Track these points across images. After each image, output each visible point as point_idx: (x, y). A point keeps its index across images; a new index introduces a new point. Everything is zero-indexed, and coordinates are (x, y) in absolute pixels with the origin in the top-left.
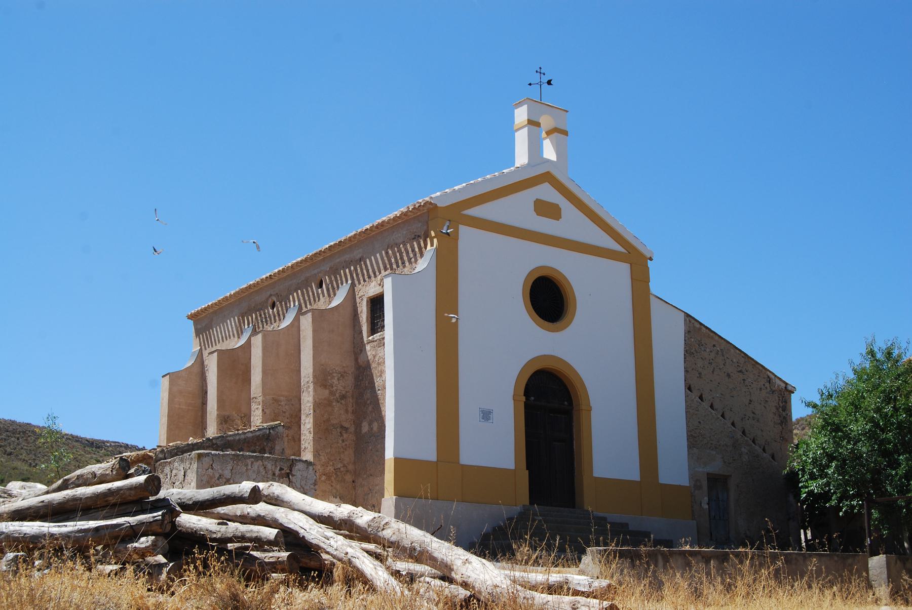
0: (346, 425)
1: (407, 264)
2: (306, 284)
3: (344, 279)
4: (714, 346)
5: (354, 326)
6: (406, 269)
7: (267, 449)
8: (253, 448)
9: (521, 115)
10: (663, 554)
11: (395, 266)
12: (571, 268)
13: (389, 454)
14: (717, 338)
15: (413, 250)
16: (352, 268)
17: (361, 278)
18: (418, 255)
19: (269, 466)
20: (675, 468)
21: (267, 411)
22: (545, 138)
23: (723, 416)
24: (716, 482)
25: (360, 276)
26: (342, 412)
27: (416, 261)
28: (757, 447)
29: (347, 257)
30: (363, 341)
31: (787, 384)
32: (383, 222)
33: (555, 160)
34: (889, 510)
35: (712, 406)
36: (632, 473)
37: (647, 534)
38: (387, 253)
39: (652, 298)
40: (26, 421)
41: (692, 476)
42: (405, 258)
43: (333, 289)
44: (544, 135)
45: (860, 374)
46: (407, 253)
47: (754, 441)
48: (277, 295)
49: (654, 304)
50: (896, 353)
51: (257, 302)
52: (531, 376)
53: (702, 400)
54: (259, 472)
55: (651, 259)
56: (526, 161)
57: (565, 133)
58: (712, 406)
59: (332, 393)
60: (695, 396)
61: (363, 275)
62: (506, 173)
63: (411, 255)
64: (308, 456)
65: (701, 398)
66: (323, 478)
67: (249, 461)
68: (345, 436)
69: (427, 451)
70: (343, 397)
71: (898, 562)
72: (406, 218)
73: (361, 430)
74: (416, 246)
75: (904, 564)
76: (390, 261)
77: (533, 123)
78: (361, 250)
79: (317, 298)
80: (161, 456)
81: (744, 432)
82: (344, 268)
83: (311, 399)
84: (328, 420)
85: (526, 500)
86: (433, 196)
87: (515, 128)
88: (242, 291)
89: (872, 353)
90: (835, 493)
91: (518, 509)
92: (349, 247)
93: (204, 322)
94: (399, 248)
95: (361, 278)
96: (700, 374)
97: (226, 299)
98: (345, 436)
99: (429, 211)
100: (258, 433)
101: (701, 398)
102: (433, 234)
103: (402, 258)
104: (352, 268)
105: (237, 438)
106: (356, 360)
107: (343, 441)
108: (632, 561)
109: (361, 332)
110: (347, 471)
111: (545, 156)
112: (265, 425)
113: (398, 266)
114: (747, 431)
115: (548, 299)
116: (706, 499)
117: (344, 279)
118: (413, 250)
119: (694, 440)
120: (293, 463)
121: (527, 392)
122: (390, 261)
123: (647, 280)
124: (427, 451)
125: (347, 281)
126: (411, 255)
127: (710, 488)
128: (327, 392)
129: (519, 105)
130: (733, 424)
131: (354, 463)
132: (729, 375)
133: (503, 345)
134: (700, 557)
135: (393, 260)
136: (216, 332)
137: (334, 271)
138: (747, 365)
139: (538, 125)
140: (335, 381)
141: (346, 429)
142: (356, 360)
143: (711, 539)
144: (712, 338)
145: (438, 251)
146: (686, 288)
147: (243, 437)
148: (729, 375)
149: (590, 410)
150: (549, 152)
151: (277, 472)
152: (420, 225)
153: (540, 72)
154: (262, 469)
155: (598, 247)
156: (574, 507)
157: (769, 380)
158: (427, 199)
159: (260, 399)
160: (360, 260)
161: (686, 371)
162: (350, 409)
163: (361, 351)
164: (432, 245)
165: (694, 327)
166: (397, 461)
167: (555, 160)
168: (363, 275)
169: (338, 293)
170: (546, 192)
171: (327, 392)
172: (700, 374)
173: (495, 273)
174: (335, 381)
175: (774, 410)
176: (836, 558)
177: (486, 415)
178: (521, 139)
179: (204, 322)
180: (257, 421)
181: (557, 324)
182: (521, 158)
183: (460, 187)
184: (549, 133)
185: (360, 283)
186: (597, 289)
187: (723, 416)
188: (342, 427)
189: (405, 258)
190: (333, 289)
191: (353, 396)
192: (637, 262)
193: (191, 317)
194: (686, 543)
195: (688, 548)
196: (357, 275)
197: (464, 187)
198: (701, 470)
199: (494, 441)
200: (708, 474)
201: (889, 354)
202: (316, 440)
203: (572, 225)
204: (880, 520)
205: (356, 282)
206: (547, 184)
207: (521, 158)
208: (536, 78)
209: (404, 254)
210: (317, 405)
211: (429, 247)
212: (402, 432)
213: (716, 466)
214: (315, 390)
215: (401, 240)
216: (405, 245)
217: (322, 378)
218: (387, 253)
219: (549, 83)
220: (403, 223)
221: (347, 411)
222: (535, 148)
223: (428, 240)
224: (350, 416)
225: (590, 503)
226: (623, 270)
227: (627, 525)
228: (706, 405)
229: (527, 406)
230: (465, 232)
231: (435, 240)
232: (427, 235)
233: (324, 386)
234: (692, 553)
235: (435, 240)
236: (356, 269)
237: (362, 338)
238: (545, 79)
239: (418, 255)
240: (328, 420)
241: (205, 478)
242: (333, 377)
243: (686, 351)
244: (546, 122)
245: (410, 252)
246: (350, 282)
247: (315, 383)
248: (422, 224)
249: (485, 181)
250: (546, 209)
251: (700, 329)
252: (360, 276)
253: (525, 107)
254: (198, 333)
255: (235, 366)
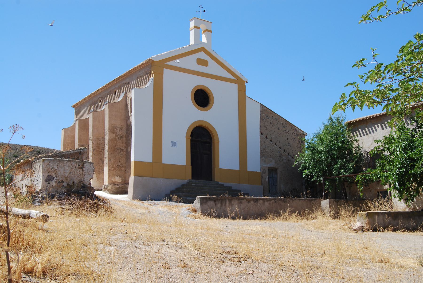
0: (123, 148)
2: (110, 93)
7: (80, 157)
8: (74, 157)
9: (192, 24)
10: (229, 199)
13: (132, 160)
15: (146, 79)
19: (74, 164)
20: (255, 164)
21: (95, 143)
23: (276, 144)
24: (272, 171)
27: (147, 83)
28: (290, 157)
29: (124, 82)
31: (303, 132)
34: (332, 181)
35: (271, 141)
36: (236, 167)
37: (239, 191)
38: (137, 80)
39: (247, 98)
41: (261, 168)
42: (143, 82)
44: (202, 32)
45: (326, 128)
47: (288, 154)
48: (101, 98)
49: (247, 100)
50: (341, 119)
51: (94, 100)
52: (193, 130)
54: (69, 166)
55: (247, 82)
56: (193, 43)
57: (211, 31)
58: (271, 141)
59: (117, 136)
60: (264, 137)
62: (185, 48)
64: (90, 160)
65: (266, 137)
66: (113, 169)
67: (65, 162)
68: (122, 152)
69: (148, 158)
70: (121, 137)
71: (335, 202)
75: (337, 203)
77: (196, 27)
79: (114, 99)
80: (34, 160)
81: (284, 151)
82: (123, 86)
83: (108, 138)
84: (115, 146)
88: (92, 94)
89: (331, 119)
90: (315, 175)
91: (187, 181)
93: (78, 108)
97: (84, 99)
98: (122, 152)
100: (76, 151)
101: (266, 137)
103: (142, 82)
105: (67, 153)
106: (127, 124)
107: (121, 154)
108: (5, 187)
109: (128, 112)
112: (79, 148)
114: (286, 151)
115: (202, 98)
116: (268, 177)
118: (146, 79)
119: (263, 154)
120: (84, 163)
121: (192, 135)
123: (245, 91)
124: (148, 158)
127: (270, 173)
128: (115, 135)
129: (191, 20)
133: (181, 117)
134: (245, 200)
136: (82, 112)
137: (120, 88)
138: (286, 124)
139: (199, 28)
140: (118, 131)
141: (122, 150)
142: (127, 122)
143: (269, 193)
145: (154, 79)
146: (265, 93)
147: (69, 153)
148: (278, 128)
150: (204, 40)
151: (77, 167)
153: (385, 2)
154: (70, 165)
157: (296, 131)
158: (150, 58)
159: (92, 138)
161: (260, 127)
162: (124, 142)
166: (135, 162)
169: (121, 96)
170: (202, 55)
171: (115, 135)
173: (178, 88)
175: (298, 142)
176: (307, 201)
177: (174, 144)
178: (192, 34)
179: (78, 108)
180: (77, 147)
182: (192, 41)
184: (204, 32)
187: (276, 144)
188: (121, 149)
189: (143, 82)
192: (241, 84)
193: (74, 106)
194: (241, 194)
195: (242, 197)
199: (177, 154)
201: (338, 120)
202: (110, 154)
203: (213, 68)
204: (329, 186)
207: (192, 41)
210: (110, 141)
211: (151, 77)
212: (140, 150)
213: (272, 164)
214: (109, 134)
215: (142, 75)
216: (143, 77)
217: (112, 130)
218: (137, 80)
219: (204, 11)
221: (123, 143)
222: (198, 37)
224: (124, 145)
225: (217, 177)
227: (231, 187)
228: (269, 140)
229: (192, 140)
230: (166, 71)
231: (153, 75)
232: (151, 73)
233: (114, 133)
235: (153, 75)
236: (127, 87)
238: (203, 10)
240: (115, 146)
241: (46, 169)
243: (261, 119)
244: (203, 27)
247: (109, 132)
249: (175, 51)
250: (201, 62)
253: (193, 21)
254: (76, 112)
255: (84, 125)
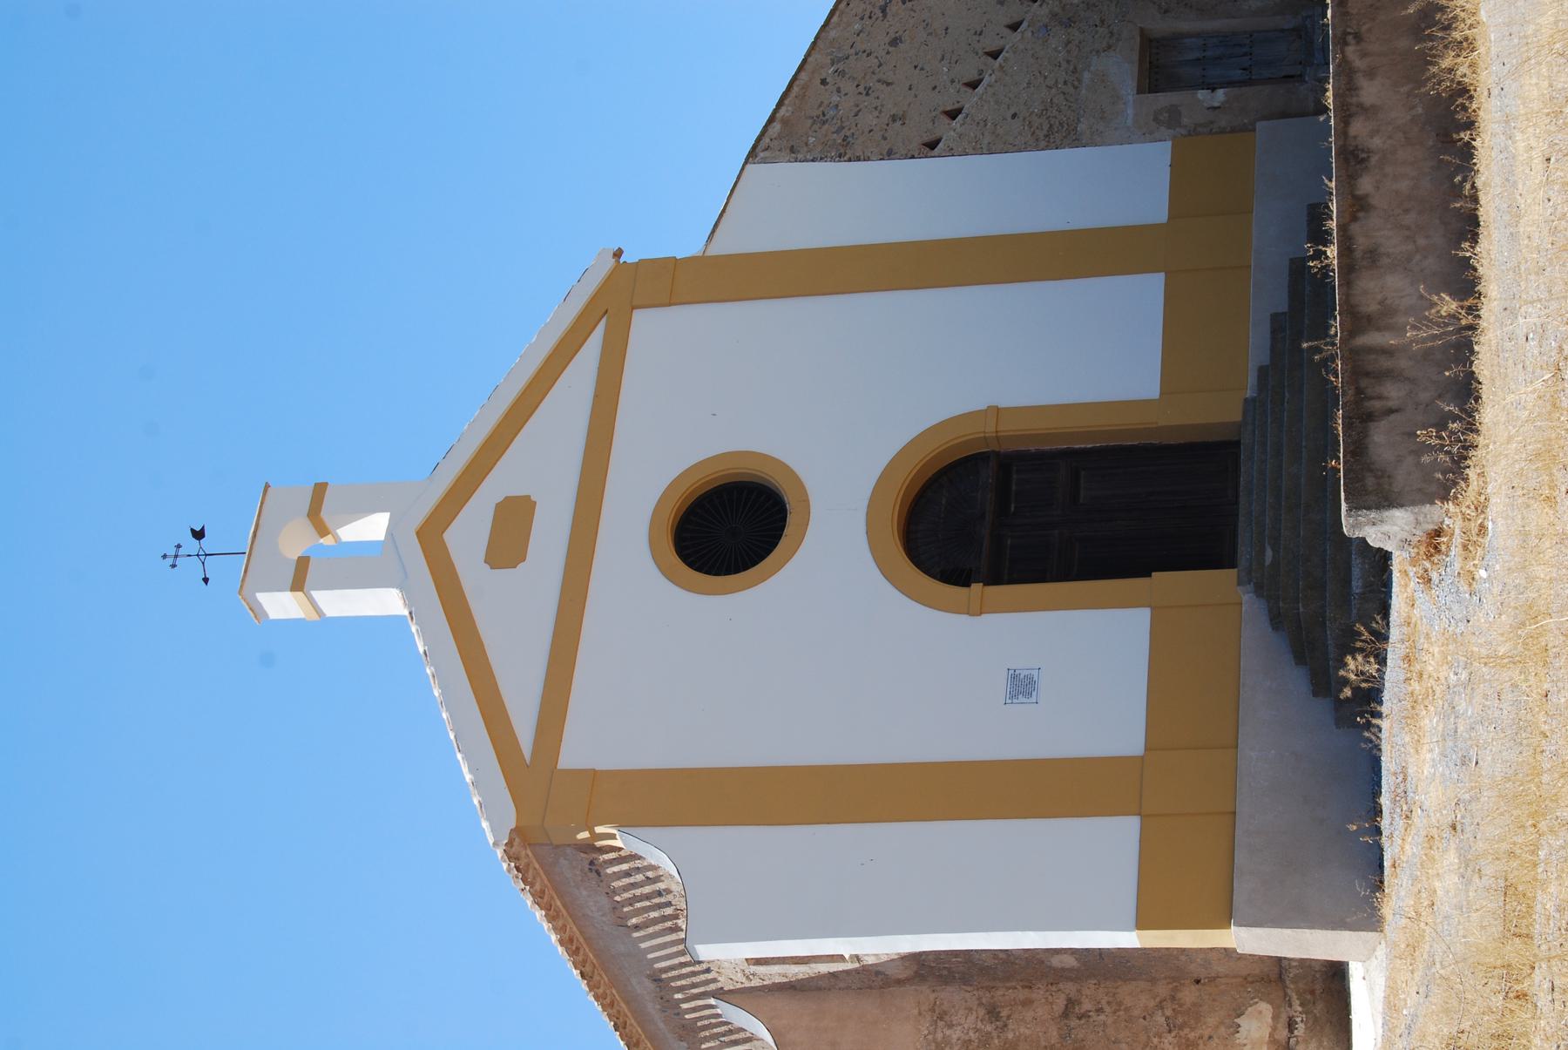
0: (1061, 1003)
1: (661, 886)
3: (707, 1012)
4: (824, 82)
5: (819, 989)
6: (674, 887)
9: (281, 605)
11: (669, 911)
12: (655, 465)
13: (1129, 940)
14: (803, 75)
15: (627, 874)
16: (678, 996)
17: (703, 977)
18: (638, 863)
20: (1124, 180)
22: (337, 538)
23: (995, 55)
24: (1160, 69)
25: (696, 979)
26: (1029, 1015)
29: (653, 1008)
30: (856, 970)
32: (561, 942)
33: (387, 515)
35: (973, 85)
37: (1298, 268)
38: (637, 927)
40: (987, 619)
41: (1148, 136)
42: (647, 889)
43: (731, 1032)
44: (327, 541)
46: (634, 886)
53: (959, 111)
55: (618, 254)
57: (320, 490)
58: (973, 85)
60: (950, 131)
61: (694, 974)
63: (640, 877)
65: (953, 115)
68: (1087, 1005)
69: (1114, 841)
70: (993, 1013)
72: (549, 892)
73: (1071, 970)
74: (616, 869)
76: (655, 921)
77: (299, 580)
78: (634, 981)
82: (680, 1014)
85: (1226, 576)
86: (491, 841)
87: (315, 617)
92: (627, 1003)
94: (623, 904)
95: (703, 977)
96: (894, 118)
98: (1087, 1005)
99: (527, 843)
101: (953, 115)
102: (584, 835)
103: (648, 897)
104: (678, 996)
106: (899, 982)
107: (1100, 1011)
109: (833, 975)
110: (1173, 998)
111: (382, 538)
113: (669, 904)
115: (731, 525)
116: (1202, 94)
117: (707, 1012)
118: (627, 874)
119: (1057, 131)
121: (957, 576)
122: (655, 921)
124: (1114, 841)
125: (712, 1007)
126: (640, 877)
129: (257, 611)
130: (1014, 27)
131: (1153, 981)
132: (895, 42)
133: (848, 640)
135: (653, 915)
139: (303, 564)
140: (955, 1034)
141: (1071, 1003)
142: (899, 982)
143: (1300, 78)
144: (805, 87)
145: (625, 823)
146: (688, 174)
148: (895, 42)
149: (997, 411)
150: (372, 527)
152: (563, 861)
155: (596, 396)
156: (1237, 444)
158: (499, 852)
160: (657, 980)
161: (890, 155)
162: (1022, 994)
163: (878, 973)
164: (613, 837)
165: (780, 137)
167: (387, 515)
168: (694, 974)
170: (468, 536)
172: (894, 118)
174: (955, 1034)
177: (1022, 686)
178: (338, 603)
181: (792, 520)
182: (387, 602)
183: (465, 769)
184: (323, 531)
185: (714, 980)
186: (701, 399)
187: (995, 55)
188: (1065, 1014)
190: (731, 1032)
191: (989, 989)
192: (631, 290)
194: (1319, 255)
195: (1332, 251)
196: (694, 986)
197: (466, 758)
198: (1130, 111)
199: (1079, 665)
200: (1140, 91)
203: (543, 465)
205: (712, 987)
206: (447, 536)
207: (387, 602)
208: (190, 568)
209: (638, 892)
211: (618, 843)
213: (1121, 69)
215: (604, 900)
216: (615, 892)
218: (637, 927)
219: (199, 535)
220: (561, 897)
221: (1027, 1003)
222: (361, 568)
223: (599, 844)
224: (1039, 994)
226: (650, 329)
227: (1275, 317)
228: (970, 100)
229: (994, 579)
230: (576, 753)
231: (599, 830)
232: (589, 848)
234: (1346, 251)
235: (599, 830)
236: (681, 989)
237: (847, 972)
238: (192, 545)
239: (638, 863)
242: (947, 1041)
243: (840, 157)
244: (295, 541)
245: (632, 880)
246: (712, 1001)
248: (563, 845)
250: (510, 536)
251: (785, 122)
252: (696, 979)
253: (264, 598)
